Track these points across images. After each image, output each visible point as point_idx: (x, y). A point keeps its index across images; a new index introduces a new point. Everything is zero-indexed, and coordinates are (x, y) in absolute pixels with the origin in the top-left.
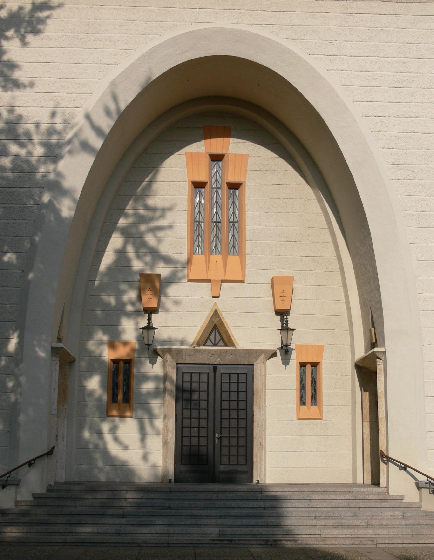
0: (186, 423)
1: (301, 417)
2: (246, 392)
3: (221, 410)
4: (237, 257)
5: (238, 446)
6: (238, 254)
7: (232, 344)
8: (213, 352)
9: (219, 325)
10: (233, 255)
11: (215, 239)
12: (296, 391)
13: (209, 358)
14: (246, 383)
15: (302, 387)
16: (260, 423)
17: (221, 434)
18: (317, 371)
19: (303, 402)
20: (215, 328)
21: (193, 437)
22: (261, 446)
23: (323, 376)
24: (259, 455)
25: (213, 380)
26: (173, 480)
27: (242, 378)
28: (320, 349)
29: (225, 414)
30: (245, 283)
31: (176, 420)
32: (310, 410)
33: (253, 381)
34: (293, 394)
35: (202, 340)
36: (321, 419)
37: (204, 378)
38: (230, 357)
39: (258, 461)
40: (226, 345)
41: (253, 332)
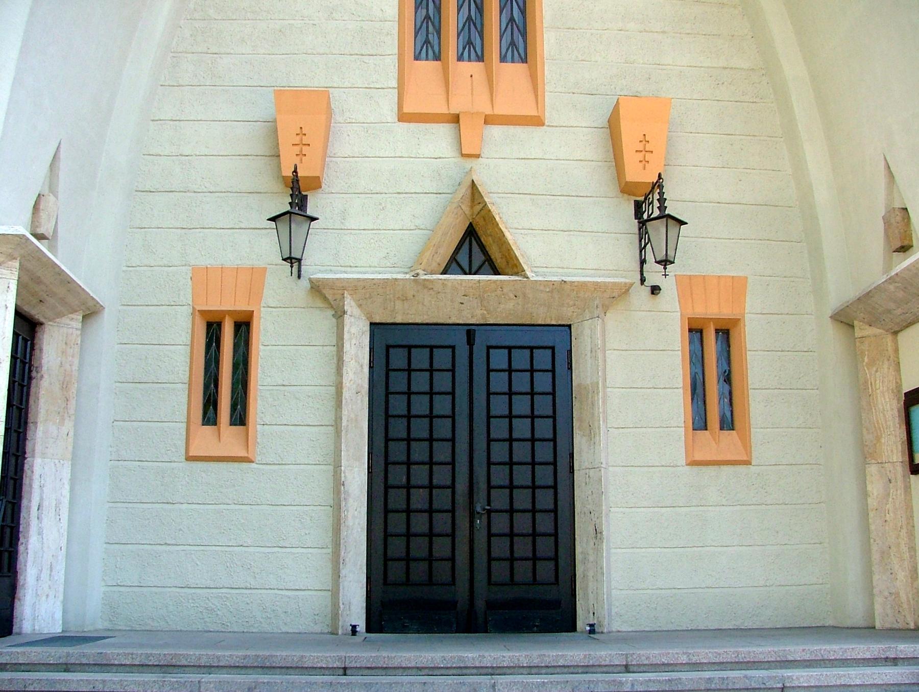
0: (397, 499)
1: (698, 457)
2: (554, 417)
3: (490, 559)
4: (520, 67)
5: (534, 487)
6: (524, 60)
7: (513, 266)
8: (465, 299)
9: (482, 222)
10: (513, 61)
11: (467, 27)
12: (681, 391)
13: (457, 305)
14: (553, 371)
15: (697, 389)
16: (592, 472)
17: (489, 505)
18: (731, 343)
19: (700, 423)
20: (471, 233)
21: (414, 393)
22: (597, 532)
23: (748, 353)
24: (591, 559)
25: (467, 561)
26: (362, 627)
27: (543, 359)
28: (738, 286)
29: (500, 476)
30: (543, 124)
31: (370, 453)
32: (717, 443)
33: (570, 368)
34: (676, 403)
35: (438, 260)
36: (747, 463)
37: (442, 358)
38: (510, 305)
39: (591, 574)
40: (497, 273)
41: (563, 239)
